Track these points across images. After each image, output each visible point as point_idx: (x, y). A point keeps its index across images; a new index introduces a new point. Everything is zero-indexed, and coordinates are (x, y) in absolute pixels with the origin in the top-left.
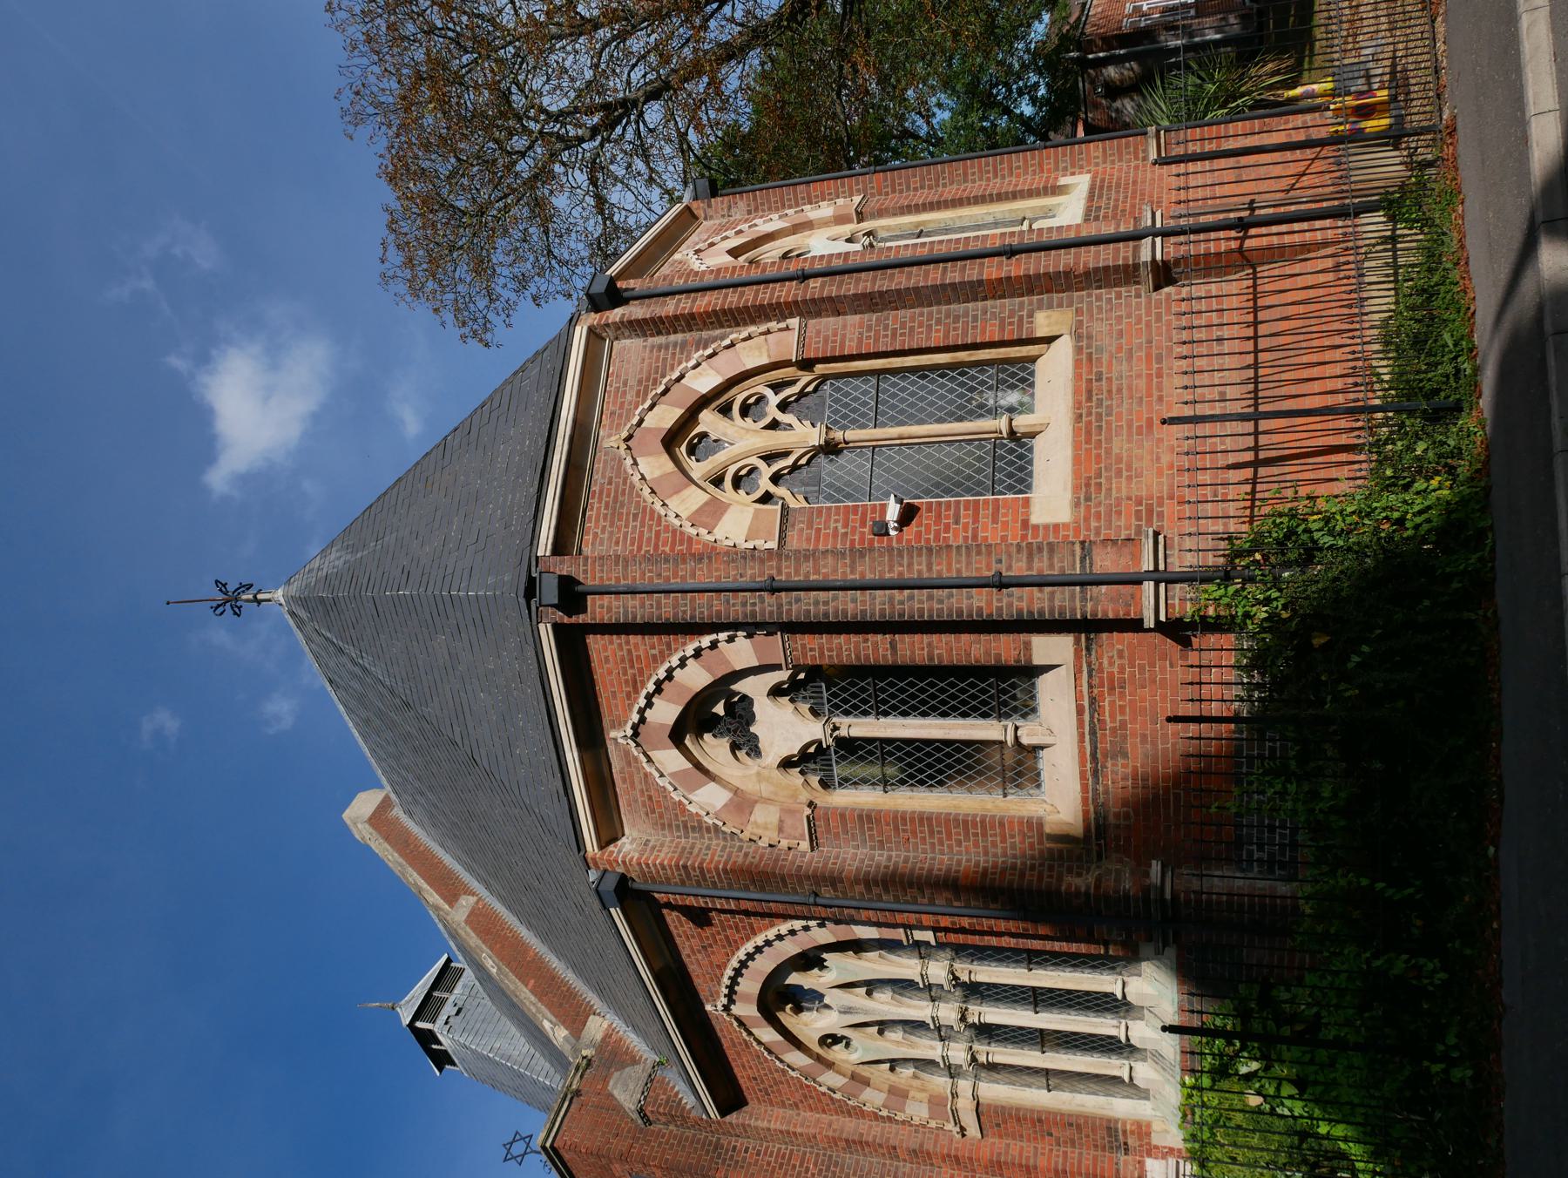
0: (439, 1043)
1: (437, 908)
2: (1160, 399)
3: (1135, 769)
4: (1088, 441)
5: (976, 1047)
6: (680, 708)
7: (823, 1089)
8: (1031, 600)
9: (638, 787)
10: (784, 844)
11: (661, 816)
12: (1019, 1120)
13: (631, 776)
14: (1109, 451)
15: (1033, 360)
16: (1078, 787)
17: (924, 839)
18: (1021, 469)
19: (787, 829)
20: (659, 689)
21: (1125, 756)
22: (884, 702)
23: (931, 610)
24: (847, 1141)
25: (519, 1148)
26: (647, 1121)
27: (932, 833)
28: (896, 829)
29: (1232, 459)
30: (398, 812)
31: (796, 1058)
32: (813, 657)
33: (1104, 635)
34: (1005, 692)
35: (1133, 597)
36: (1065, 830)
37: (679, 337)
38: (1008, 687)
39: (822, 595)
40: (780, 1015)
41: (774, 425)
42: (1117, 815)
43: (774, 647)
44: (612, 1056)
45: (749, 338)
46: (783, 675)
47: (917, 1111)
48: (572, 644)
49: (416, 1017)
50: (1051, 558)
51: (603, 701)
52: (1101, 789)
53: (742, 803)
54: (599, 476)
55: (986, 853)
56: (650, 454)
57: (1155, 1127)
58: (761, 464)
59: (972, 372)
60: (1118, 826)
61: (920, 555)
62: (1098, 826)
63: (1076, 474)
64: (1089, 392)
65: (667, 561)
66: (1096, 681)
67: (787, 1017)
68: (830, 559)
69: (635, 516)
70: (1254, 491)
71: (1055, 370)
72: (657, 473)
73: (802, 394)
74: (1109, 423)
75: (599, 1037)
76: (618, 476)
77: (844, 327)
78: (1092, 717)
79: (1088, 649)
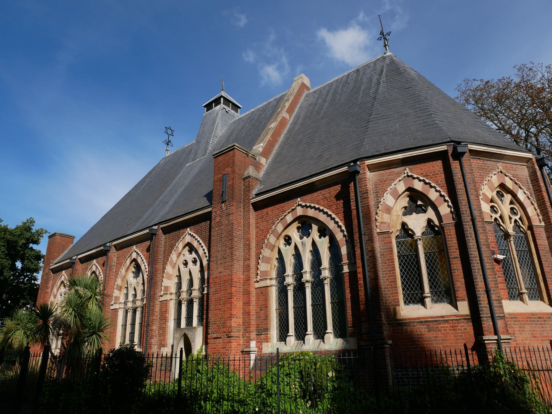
0: (215, 106)
1: (285, 107)
2: (543, 340)
3: (425, 335)
4: (527, 318)
5: (292, 286)
6: (421, 190)
7: (268, 236)
8: (484, 301)
9: (389, 177)
10: (378, 224)
11: (379, 184)
12: (265, 300)
13: (393, 175)
14: (525, 324)
15: (542, 299)
16: (415, 317)
17: (387, 268)
18: (535, 297)
19: (382, 225)
20: (426, 183)
21: (429, 331)
22: (430, 255)
23: (475, 269)
24: (250, 244)
25: (169, 132)
26: (244, 179)
27: (390, 271)
28: (389, 260)
29: (530, 363)
30: (306, 92)
31: (280, 228)
32: (447, 233)
33: (471, 324)
34: (440, 293)
35: (490, 332)
36: (398, 313)
37: (531, 187)
38: (447, 295)
39: (473, 235)
40: (297, 222)
41: (510, 218)
42: (406, 329)
43: (448, 220)
44: (258, 166)
45: (536, 210)
46: (437, 223)
47: (263, 267)
48: (442, 156)
49: (225, 98)
50: (498, 306)
51: (418, 165)
52: (416, 324)
53: (388, 210)
54: (490, 163)
55: (385, 288)
56: (498, 179)
57: (270, 344)
58: (499, 215)
59: (535, 281)
60: (402, 329)
61: (491, 266)
62: (402, 323)
63: (518, 314)
64: (540, 318)
65: (475, 186)
66: (454, 321)
67: (296, 224)
68: (484, 238)
69: (480, 175)
70: (536, 371)
71: (443, 309)
72: (493, 182)
73: (519, 227)
74: (533, 324)
75: (261, 162)
76: (490, 169)
77: (544, 240)
78: (441, 321)
79: (465, 319)
